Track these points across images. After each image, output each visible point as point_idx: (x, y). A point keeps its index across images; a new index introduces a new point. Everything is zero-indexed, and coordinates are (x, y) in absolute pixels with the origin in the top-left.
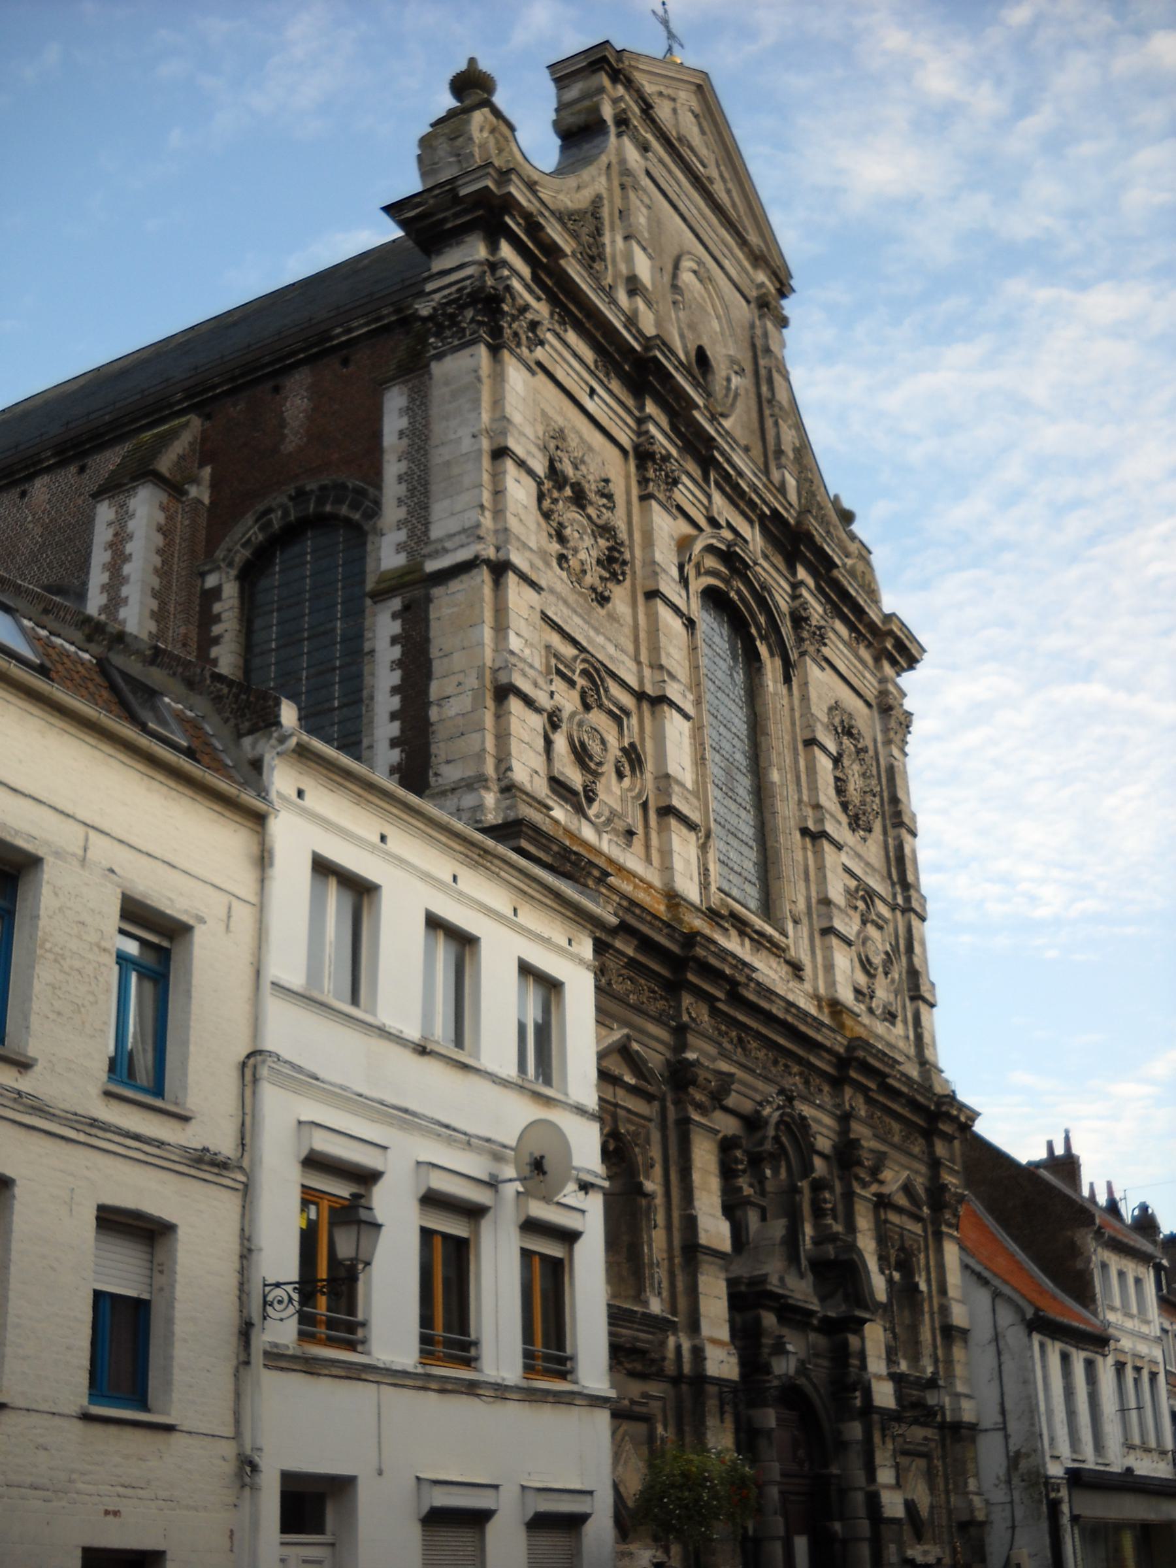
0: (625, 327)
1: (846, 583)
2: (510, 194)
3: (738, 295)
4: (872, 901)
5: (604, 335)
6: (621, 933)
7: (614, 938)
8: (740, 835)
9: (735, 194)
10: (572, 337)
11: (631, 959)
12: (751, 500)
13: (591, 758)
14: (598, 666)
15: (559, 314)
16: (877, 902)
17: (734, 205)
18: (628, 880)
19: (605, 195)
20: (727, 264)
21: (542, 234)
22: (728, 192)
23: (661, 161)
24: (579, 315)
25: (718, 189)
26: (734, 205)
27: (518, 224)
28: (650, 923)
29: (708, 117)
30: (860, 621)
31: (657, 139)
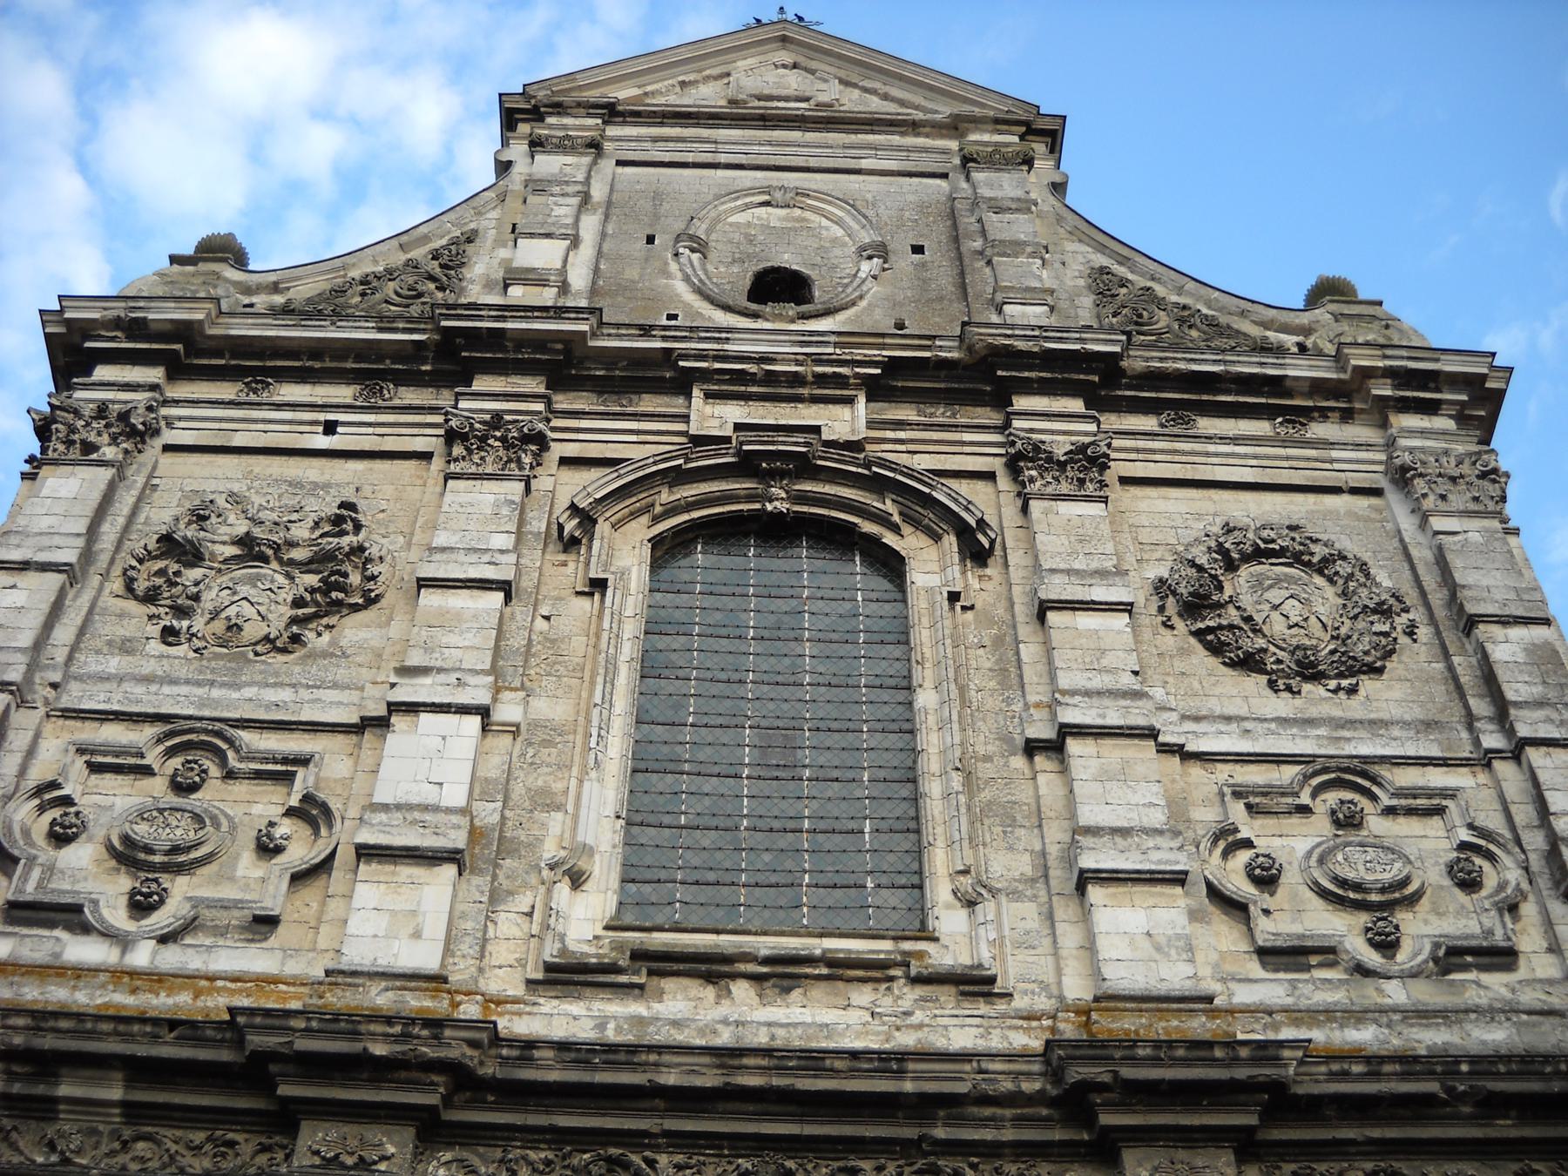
0: (381, 330)
1: (1181, 366)
2: (1356, 368)
3: (915, 180)
4: (1374, 779)
5: (358, 359)
6: (64, 1071)
7: (57, 1084)
8: (838, 826)
9: (896, 92)
10: (1206, 425)
11: (125, 1105)
12: (817, 376)
13: (149, 850)
14: (218, 726)
15: (257, 382)
16: (1384, 772)
17: (902, 103)
18: (182, 988)
19: (1102, 260)
20: (865, 164)
21: (153, 326)
22: (885, 97)
23: (655, 140)
24: (942, 385)
25: (852, 101)
26: (902, 103)
27: (112, 339)
28: (116, 1033)
29: (812, 54)
30: (1289, 394)
31: (662, 124)
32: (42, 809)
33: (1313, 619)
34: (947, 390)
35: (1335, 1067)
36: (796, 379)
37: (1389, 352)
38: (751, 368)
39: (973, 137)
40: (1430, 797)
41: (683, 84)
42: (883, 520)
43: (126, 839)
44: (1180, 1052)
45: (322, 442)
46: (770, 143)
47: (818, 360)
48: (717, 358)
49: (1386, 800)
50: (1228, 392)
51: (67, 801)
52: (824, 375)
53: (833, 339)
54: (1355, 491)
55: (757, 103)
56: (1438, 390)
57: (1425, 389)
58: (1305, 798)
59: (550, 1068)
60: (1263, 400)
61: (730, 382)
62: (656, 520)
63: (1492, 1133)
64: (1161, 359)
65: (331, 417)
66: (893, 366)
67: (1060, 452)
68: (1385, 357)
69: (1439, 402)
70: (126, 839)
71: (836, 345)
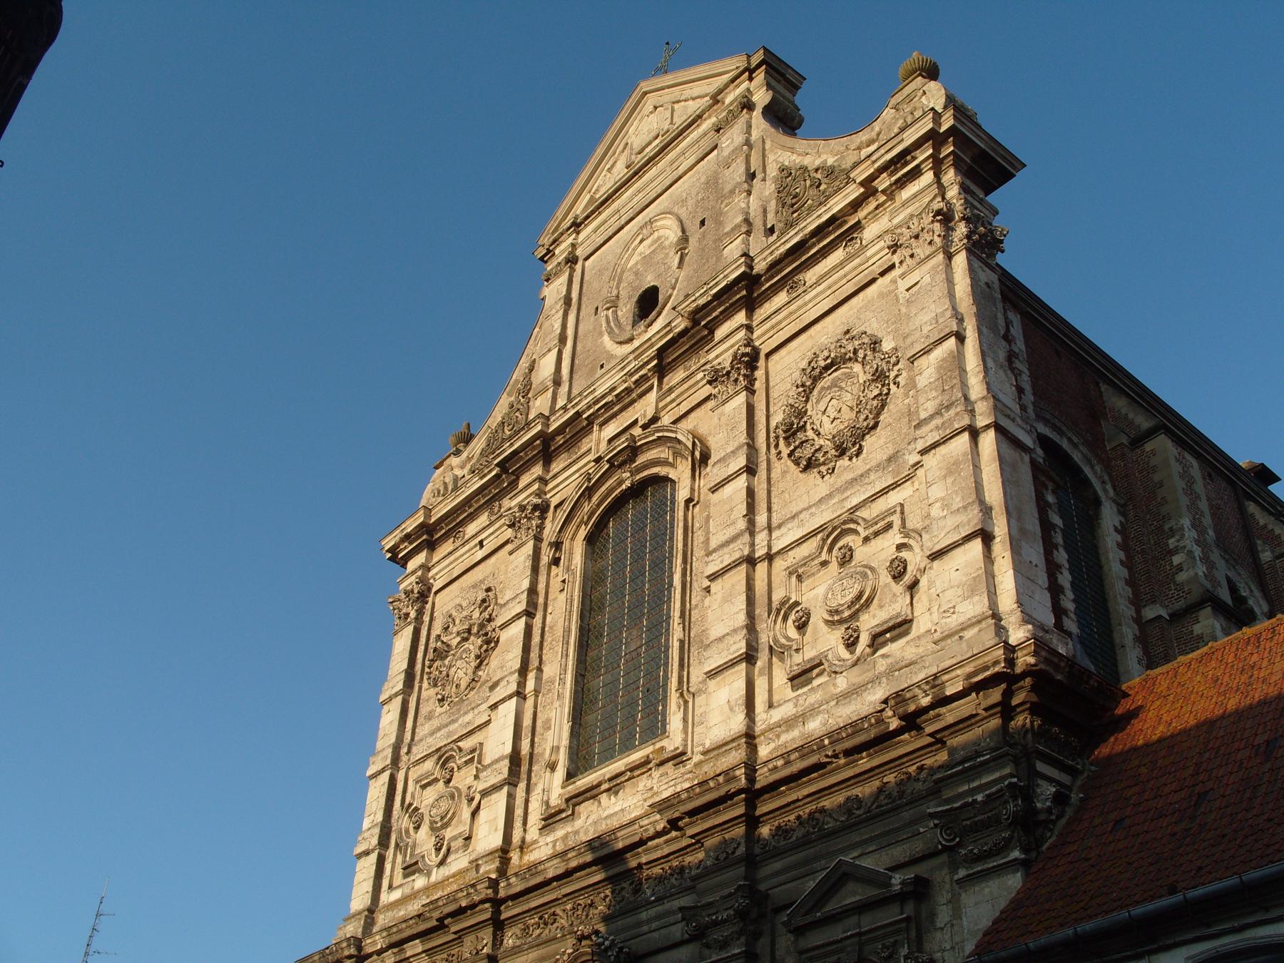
0: (481, 478)
10: (811, 275)
23: (595, 231)
32: (785, 618)
33: (844, 408)
34: (691, 347)
35: (770, 766)
36: (628, 391)
37: (874, 158)
38: (609, 398)
39: (727, 101)
40: (883, 519)
41: (609, 170)
42: (665, 463)
43: (831, 613)
44: (698, 790)
45: (480, 554)
46: (639, 192)
47: (631, 374)
48: (595, 403)
49: (863, 534)
50: (814, 245)
51: (797, 603)
52: (636, 381)
53: (632, 357)
54: (882, 274)
55: (640, 156)
56: (914, 158)
57: (906, 164)
58: (824, 556)
59: (911, 742)
60: (832, 237)
61: (606, 411)
62: (586, 524)
63: (857, 770)
64: (771, 253)
65: (480, 538)
66: (661, 353)
67: (727, 365)
68: (874, 162)
69: (918, 166)
70: (831, 613)
71: (635, 359)
